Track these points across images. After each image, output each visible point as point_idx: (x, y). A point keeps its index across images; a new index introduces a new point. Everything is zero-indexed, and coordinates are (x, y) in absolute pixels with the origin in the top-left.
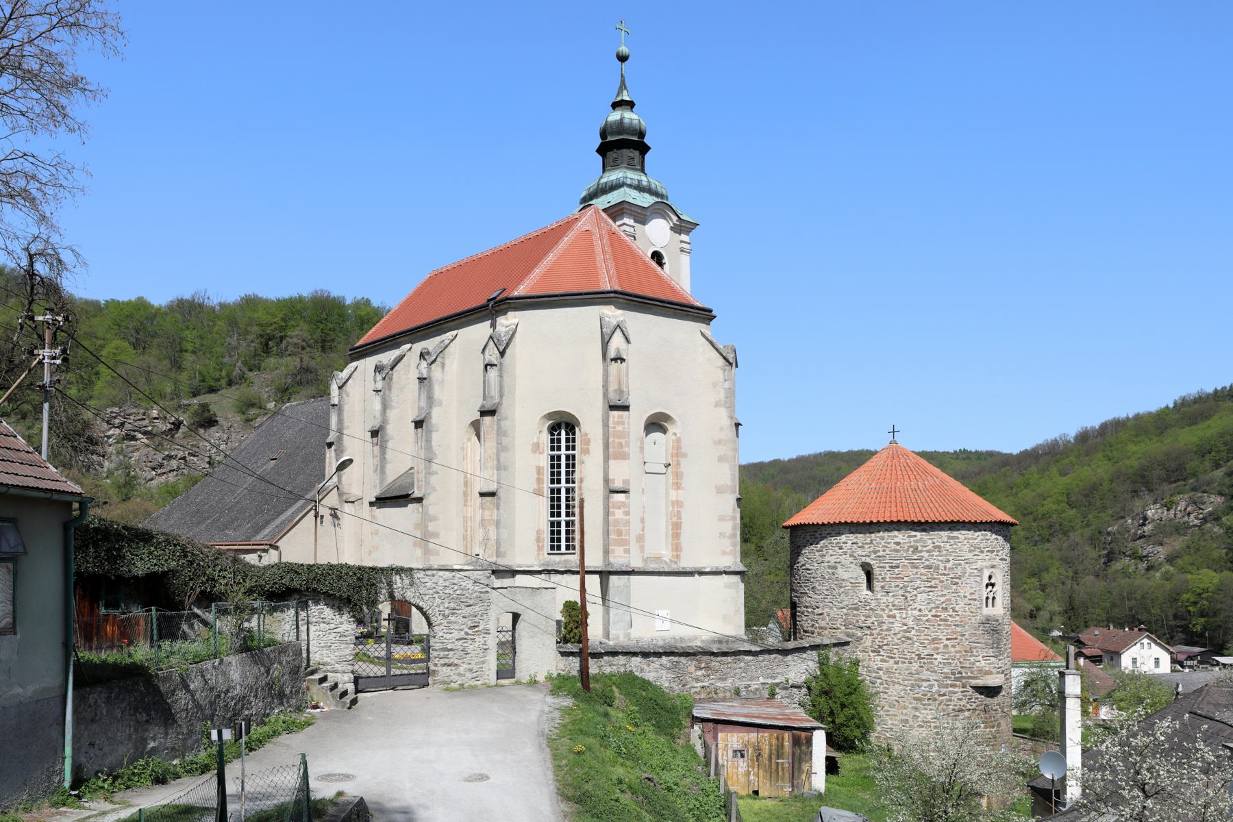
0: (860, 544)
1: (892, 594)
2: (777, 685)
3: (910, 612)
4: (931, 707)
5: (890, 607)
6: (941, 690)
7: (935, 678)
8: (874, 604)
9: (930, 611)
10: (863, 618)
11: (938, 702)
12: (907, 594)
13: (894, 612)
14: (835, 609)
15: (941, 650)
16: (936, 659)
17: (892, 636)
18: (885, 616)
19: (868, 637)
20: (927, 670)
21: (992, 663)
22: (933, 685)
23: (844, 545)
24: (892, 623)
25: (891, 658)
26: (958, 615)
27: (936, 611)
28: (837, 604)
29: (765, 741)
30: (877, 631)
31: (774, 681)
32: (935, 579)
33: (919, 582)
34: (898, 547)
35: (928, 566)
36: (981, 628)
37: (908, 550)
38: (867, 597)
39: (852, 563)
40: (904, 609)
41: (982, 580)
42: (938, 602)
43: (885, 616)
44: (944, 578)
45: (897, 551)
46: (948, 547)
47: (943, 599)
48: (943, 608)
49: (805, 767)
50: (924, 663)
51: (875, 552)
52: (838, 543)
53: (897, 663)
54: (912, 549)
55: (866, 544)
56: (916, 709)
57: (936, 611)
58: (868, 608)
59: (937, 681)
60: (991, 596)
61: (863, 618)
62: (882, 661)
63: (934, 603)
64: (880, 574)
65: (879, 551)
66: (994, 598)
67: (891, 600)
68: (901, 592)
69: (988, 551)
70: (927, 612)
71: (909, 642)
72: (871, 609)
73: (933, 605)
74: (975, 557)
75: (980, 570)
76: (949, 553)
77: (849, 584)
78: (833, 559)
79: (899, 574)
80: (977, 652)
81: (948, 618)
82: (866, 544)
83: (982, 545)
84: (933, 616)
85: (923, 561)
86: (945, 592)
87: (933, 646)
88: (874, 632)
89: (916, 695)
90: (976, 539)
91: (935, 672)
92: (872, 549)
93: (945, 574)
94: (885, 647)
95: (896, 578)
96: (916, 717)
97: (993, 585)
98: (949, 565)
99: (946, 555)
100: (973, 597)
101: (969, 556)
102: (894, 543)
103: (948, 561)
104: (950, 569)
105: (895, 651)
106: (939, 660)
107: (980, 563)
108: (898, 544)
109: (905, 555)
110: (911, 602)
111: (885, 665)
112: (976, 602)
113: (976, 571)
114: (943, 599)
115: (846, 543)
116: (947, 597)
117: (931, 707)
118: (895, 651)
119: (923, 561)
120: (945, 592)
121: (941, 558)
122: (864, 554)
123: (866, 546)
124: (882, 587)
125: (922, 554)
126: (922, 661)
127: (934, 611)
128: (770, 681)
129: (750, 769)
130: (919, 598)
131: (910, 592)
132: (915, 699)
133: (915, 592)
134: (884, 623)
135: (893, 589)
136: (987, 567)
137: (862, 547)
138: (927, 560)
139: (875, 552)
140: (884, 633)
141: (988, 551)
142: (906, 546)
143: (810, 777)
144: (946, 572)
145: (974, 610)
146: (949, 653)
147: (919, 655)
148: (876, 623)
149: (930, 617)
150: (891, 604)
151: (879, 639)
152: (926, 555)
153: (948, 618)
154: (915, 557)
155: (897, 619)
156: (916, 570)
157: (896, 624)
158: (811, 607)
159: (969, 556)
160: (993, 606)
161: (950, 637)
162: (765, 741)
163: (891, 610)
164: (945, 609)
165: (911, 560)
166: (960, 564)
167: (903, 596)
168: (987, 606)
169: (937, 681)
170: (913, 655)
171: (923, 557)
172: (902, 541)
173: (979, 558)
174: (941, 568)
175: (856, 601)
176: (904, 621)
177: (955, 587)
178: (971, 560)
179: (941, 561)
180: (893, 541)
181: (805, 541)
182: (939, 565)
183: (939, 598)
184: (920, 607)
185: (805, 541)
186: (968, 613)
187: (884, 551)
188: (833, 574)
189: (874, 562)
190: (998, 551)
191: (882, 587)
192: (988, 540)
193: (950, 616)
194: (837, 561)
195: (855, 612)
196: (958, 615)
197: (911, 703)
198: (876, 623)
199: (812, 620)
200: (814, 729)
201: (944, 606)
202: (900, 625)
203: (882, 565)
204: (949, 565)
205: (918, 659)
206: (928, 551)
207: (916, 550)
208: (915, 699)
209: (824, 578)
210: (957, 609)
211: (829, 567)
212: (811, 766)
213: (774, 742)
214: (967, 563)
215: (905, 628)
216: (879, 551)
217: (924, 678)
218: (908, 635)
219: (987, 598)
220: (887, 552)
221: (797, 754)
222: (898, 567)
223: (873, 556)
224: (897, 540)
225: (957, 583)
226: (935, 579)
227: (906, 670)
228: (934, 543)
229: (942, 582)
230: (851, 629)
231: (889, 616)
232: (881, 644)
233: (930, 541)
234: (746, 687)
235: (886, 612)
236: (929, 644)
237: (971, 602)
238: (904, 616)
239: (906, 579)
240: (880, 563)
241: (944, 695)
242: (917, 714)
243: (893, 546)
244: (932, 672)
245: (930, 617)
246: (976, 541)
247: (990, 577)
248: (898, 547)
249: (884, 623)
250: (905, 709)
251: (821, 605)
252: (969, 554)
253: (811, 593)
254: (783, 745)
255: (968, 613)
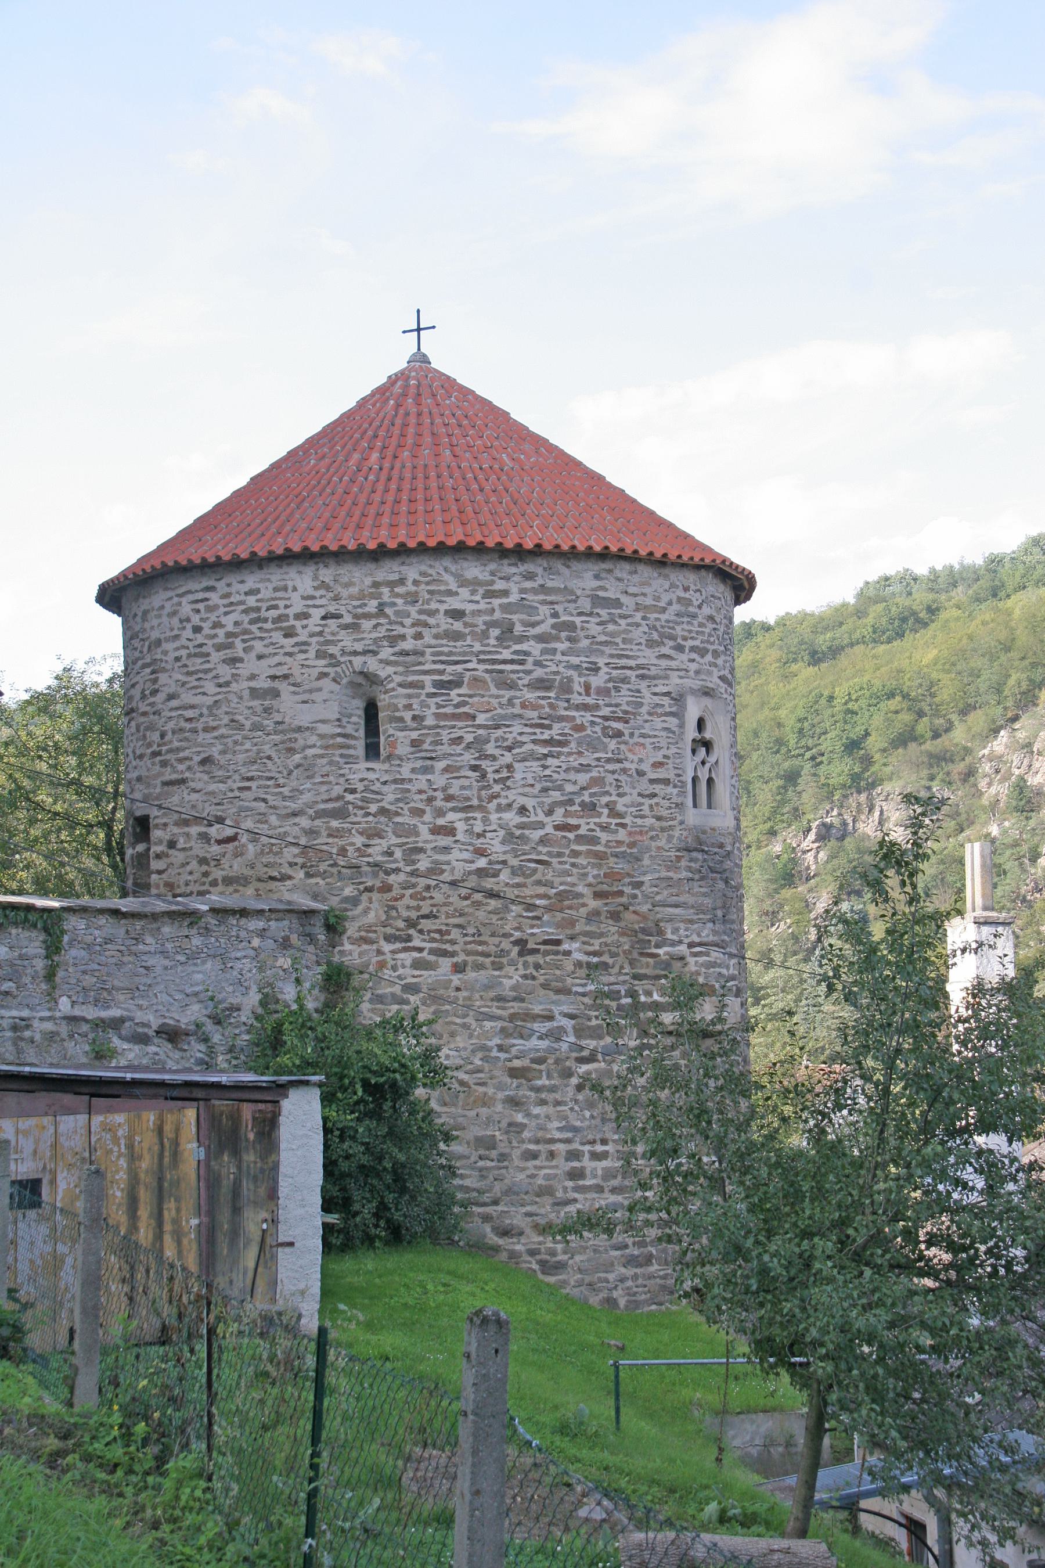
0: (348, 619)
1: (440, 765)
2: (116, 1024)
3: (494, 817)
4: (558, 1096)
5: (439, 803)
6: (584, 1043)
7: (565, 1009)
8: (391, 797)
9: (550, 813)
10: (359, 840)
11: (574, 1081)
12: (484, 764)
13: (451, 816)
14: (273, 819)
15: (579, 928)
16: (568, 953)
17: (445, 888)
18: (424, 830)
19: (375, 896)
20: (545, 986)
21: (713, 965)
22: (562, 1029)
23: (298, 624)
24: (446, 850)
25: (445, 953)
26: (623, 826)
27: (567, 814)
28: (279, 803)
29: (116, 1140)
30: (402, 877)
31: (104, 1014)
32: (561, 719)
33: (517, 728)
34: (458, 626)
35: (541, 680)
36: (683, 863)
37: (485, 634)
38: (372, 776)
39: (323, 675)
40: (481, 808)
41: (682, 726)
42: (569, 788)
43: (424, 830)
44: (583, 717)
45: (457, 636)
46: (594, 629)
47: (583, 778)
48: (583, 804)
49: (253, 1222)
50: (537, 966)
51: (394, 640)
52: (280, 619)
53: (459, 969)
54: (495, 632)
55: (367, 616)
56: (514, 1102)
57: (567, 814)
58: (373, 808)
59: (572, 1017)
60: (703, 775)
61: (359, 840)
62: (417, 965)
63: (560, 788)
64: (408, 707)
65: (403, 637)
66: (710, 781)
67: (440, 781)
68: (469, 758)
69: (693, 649)
70: (541, 817)
71: (493, 903)
72: (383, 811)
73: (556, 796)
74: (664, 663)
75: (679, 699)
76: (596, 646)
77: (313, 739)
78: (264, 669)
79: (464, 704)
80: (675, 931)
81: (599, 833)
82: (367, 616)
83: (679, 631)
84: (557, 828)
85: (529, 666)
86: (588, 758)
87: (559, 916)
88: (392, 879)
89: (517, 1063)
90: (664, 610)
91: (566, 991)
92: (382, 632)
93: (586, 707)
94: (426, 925)
95: (455, 716)
96: (516, 1129)
97: (707, 745)
98: (597, 681)
99: (589, 651)
100: (661, 774)
101: (648, 656)
102: (446, 612)
103: (595, 669)
104: (600, 691)
105: (455, 934)
106: (578, 956)
107: (675, 679)
108: (457, 614)
109: (477, 647)
110: (497, 788)
111: (427, 977)
112: (670, 789)
113: (666, 701)
114: (583, 778)
115: (306, 616)
116: (594, 774)
117: (558, 1096)
118: (455, 934)
119: (529, 666)
120: (588, 758)
121: (575, 660)
122: (359, 647)
123: (367, 625)
124: (415, 744)
125: (524, 647)
126: (530, 959)
127: (560, 811)
128: (91, 1013)
129: (61, 1248)
130: (518, 776)
131: (494, 758)
132: (514, 1073)
133: (508, 758)
134: (421, 850)
135: (446, 748)
136: (693, 692)
137: (354, 627)
138: (538, 663)
139: (394, 640)
140: (423, 882)
141: (693, 649)
142: (480, 620)
143: (274, 1257)
144: (589, 700)
145: (665, 813)
146: (601, 935)
147: (521, 943)
148: (398, 854)
149: (549, 829)
150: (439, 795)
151: (407, 901)
152: (535, 648)
153: (599, 833)
154: (506, 655)
155: (460, 836)
156: (508, 694)
157: (456, 854)
158: (198, 820)
159: (648, 656)
160: (709, 806)
161: (605, 887)
162: (116, 1140)
163: (440, 813)
164: (590, 808)
165: (494, 662)
166: (625, 680)
167: (474, 768)
168: (695, 806)
169: (572, 1017)
170: (506, 945)
171: (526, 653)
172: (469, 607)
173: (673, 664)
174: (577, 687)
175: (338, 790)
176: (479, 842)
177: (612, 744)
178: (653, 671)
179: (577, 667)
180: (443, 608)
181: (175, 621)
182: (570, 680)
183: (572, 776)
184: (522, 801)
185: (175, 621)
186: (650, 821)
187: (418, 636)
188: (267, 710)
189: (390, 670)
190: (716, 654)
191: (415, 744)
192: (694, 616)
193: (605, 828)
194: (279, 671)
195: (335, 824)
196: (623, 826)
197: (500, 1087)
198: (398, 854)
199: (203, 861)
200: (282, 1089)
201: (586, 798)
202: (466, 855)
203: (411, 678)
204: (597, 681)
205: (521, 954)
206: (541, 638)
207: (507, 633)
208: (514, 1073)
209: (241, 727)
210: (620, 808)
211: (254, 693)
212: (274, 1222)
213: (147, 1141)
214: (643, 677)
215: (482, 863)
216: (403, 637)
217: (537, 1009)
218: (489, 883)
219: (695, 780)
220: (428, 639)
221: (227, 1183)
222: (457, 684)
223: (386, 653)
224: (454, 603)
225: (619, 734)
226: (561, 719)
227: (487, 987)
228: (555, 615)
229: (580, 728)
230: (323, 875)
231: (436, 831)
232: (414, 915)
233: (544, 610)
234: (15, 1028)
235: (428, 817)
236: (548, 909)
237: (658, 788)
238: (478, 828)
239: (481, 719)
240: (407, 673)
241: (591, 1059)
242: (520, 1118)
243: (444, 623)
244: (558, 991)
245: (549, 829)
246: (664, 617)
247: (701, 724)
248: (458, 626)
249: (421, 850)
250: (484, 1104)
251: (230, 811)
252: (648, 652)
253: (199, 779)
254: (176, 1154)
255: (650, 821)
